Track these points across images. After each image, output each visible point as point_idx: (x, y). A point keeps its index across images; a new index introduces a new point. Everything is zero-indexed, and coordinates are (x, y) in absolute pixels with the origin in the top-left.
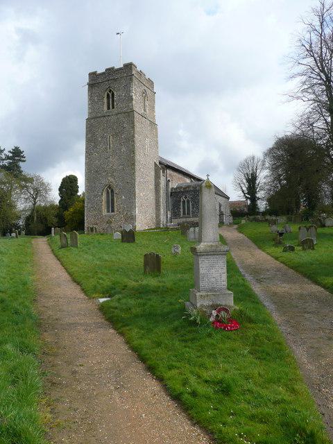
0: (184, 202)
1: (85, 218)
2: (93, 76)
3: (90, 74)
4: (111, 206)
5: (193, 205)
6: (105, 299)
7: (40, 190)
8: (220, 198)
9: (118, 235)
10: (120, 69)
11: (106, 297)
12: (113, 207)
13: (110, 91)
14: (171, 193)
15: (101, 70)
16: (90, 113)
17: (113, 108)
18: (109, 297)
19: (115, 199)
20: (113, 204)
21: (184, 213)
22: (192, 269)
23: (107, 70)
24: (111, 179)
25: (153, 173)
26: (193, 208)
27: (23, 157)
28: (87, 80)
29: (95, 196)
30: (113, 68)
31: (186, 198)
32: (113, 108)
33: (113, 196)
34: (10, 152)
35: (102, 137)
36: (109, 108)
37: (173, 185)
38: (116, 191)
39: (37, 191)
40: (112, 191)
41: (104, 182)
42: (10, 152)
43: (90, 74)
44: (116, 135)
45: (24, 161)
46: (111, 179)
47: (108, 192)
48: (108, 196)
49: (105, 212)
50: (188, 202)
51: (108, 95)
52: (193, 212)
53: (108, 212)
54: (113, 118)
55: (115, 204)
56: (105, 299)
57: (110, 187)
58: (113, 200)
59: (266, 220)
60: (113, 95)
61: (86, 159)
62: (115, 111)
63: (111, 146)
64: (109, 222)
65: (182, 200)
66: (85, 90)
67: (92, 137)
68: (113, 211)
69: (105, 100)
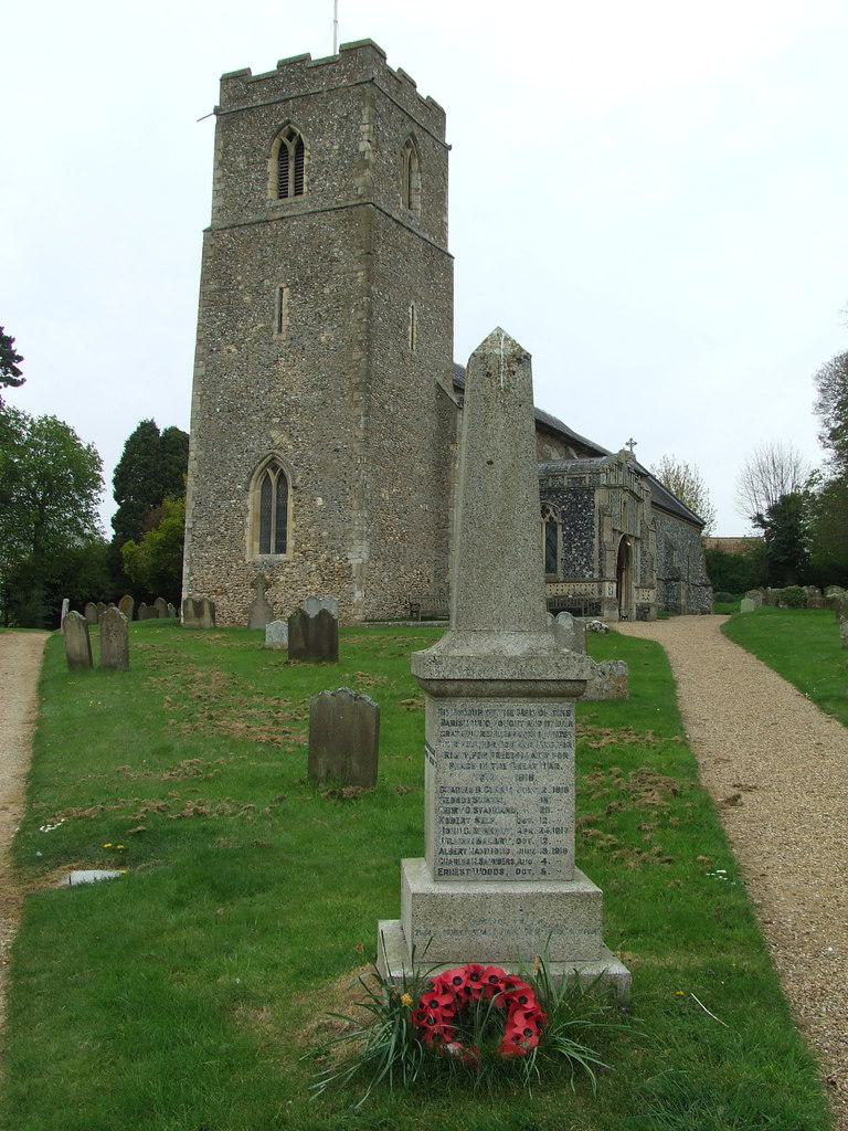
1: (186, 570)
2: (237, 85)
3: (226, 80)
4: (274, 532)
5: (568, 538)
6: (99, 874)
8: (670, 521)
9: (277, 633)
10: (328, 62)
11: (101, 867)
12: (282, 535)
13: (291, 135)
15: (263, 65)
16: (218, 211)
18: (120, 865)
19: (291, 505)
20: (282, 522)
22: (591, 493)
23: (282, 64)
25: (430, 422)
26: (568, 550)
27: (17, 372)
28: (214, 99)
29: (221, 494)
30: (305, 58)
32: (298, 191)
33: (283, 496)
36: (283, 194)
38: (296, 477)
39: (158, 553)
40: (282, 478)
43: (226, 80)
44: (303, 285)
45: (16, 384)
48: (265, 496)
49: (252, 553)
51: (283, 148)
52: (568, 565)
53: (265, 549)
55: (291, 525)
56: (99, 874)
58: (282, 509)
59: (831, 603)
60: (300, 147)
61: (196, 367)
62: (304, 202)
63: (286, 322)
66: (203, 139)
68: (281, 549)
69: (272, 166)
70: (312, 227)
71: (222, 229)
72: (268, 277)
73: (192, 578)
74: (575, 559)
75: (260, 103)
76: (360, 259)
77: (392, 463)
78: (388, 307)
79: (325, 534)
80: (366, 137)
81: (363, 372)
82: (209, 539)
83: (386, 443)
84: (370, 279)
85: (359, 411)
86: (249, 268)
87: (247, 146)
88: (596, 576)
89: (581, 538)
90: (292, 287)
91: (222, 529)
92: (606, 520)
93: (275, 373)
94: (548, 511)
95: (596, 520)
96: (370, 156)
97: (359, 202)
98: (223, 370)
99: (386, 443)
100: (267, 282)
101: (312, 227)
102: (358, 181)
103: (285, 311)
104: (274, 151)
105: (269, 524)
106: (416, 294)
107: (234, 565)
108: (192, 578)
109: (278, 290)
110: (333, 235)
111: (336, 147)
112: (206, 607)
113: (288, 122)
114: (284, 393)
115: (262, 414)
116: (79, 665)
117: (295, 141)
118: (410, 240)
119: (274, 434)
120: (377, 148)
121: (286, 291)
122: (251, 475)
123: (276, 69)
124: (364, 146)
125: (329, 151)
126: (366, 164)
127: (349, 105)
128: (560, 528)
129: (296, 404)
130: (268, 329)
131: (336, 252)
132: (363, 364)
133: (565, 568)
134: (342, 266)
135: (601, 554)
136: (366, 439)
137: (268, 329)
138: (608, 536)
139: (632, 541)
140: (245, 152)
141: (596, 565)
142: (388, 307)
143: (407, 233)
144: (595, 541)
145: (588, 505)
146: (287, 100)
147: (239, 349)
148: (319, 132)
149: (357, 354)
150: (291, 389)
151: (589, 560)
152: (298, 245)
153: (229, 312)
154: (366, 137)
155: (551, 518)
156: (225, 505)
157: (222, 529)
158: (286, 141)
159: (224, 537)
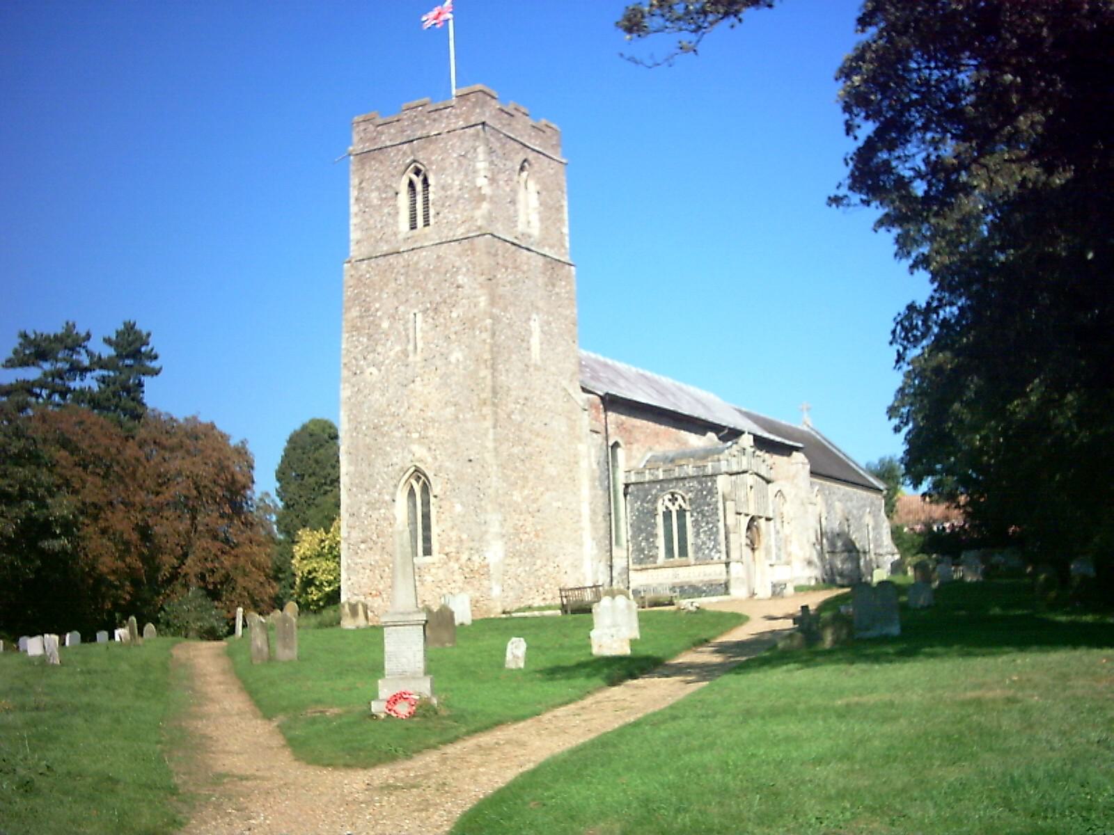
0: (667, 515)
5: (696, 523)
7: (1038, 174)
12: (427, 540)
14: (627, 486)
17: (427, 224)
20: (427, 527)
21: (669, 552)
24: (419, 451)
26: (697, 535)
29: (372, 505)
31: (673, 499)
32: (427, 224)
33: (426, 504)
34: (108, 341)
35: (392, 317)
36: (413, 227)
37: (630, 462)
38: (436, 489)
41: (402, 459)
42: (108, 341)
45: (156, 372)
46: (419, 451)
47: (412, 493)
50: (681, 513)
52: (698, 549)
54: (424, 259)
57: (418, 474)
58: (426, 517)
63: (420, 345)
64: (188, 477)
65: (661, 509)
67: (361, 317)
69: (404, 199)
70: (439, 257)
71: (360, 261)
72: (402, 303)
73: (349, 583)
74: (704, 543)
75: (388, 143)
76: (482, 286)
77: (522, 468)
78: (510, 325)
79: (464, 536)
80: (482, 173)
81: (488, 389)
82: (363, 546)
83: (516, 450)
84: (493, 302)
85: (488, 423)
86: (385, 296)
87: (378, 182)
88: (724, 557)
89: (707, 523)
90: (425, 312)
91: (374, 537)
92: (729, 504)
93: (412, 391)
94: (676, 499)
95: (720, 505)
96: (487, 191)
97: (478, 233)
98: (367, 391)
99: (516, 450)
100: (402, 309)
101: (439, 257)
102: (478, 213)
103: (419, 335)
104: (403, 187)
105: (416, 530)
106: (537, 308)
107: (387, 569)
108: (349, 583)
109: (412, 316)
110: (457, 264)
111: (457, 183)
112: (360, 608)
113: (415, 161)
114: (421, 410)
115: (402, 430)
116: (580, 648)
117: (421, 178)
118: (529, 258)
119: (415, 448)
120: (493, 180)
121: (419, 316)
122: (396, 486)
123: (98, 635)
124: (481, 182)
125: (451, 186)
126: (482, 198)
127: (466, 145)
128: (688, 514)
129: (433, 420)
130: (405, 353)
131: (460, 279)
132: (489, 381)
133: (696, 552)
134: (467, 291)
135: (727, 538)
136: (496, 449)
137: (405, 353)
138: (731, 519)
139: (762, 521)
140: (378, 189)
141: (723, 548)
142: (510, 325)
143: (525, 252)
144: (721, 525)
145: (712, 492)
146: (412, 141)
147: (380, 370)
148: (442, 170)
149: (485, 373)
150: (427, 406)
151: (717, 543)
152: (427, 273)
153: (370, 336)
154: (482, 173)
155: (680, 507)
156: (375, 515)
157: (374, 537)
158: (414, 177)
159: (375, 543)
